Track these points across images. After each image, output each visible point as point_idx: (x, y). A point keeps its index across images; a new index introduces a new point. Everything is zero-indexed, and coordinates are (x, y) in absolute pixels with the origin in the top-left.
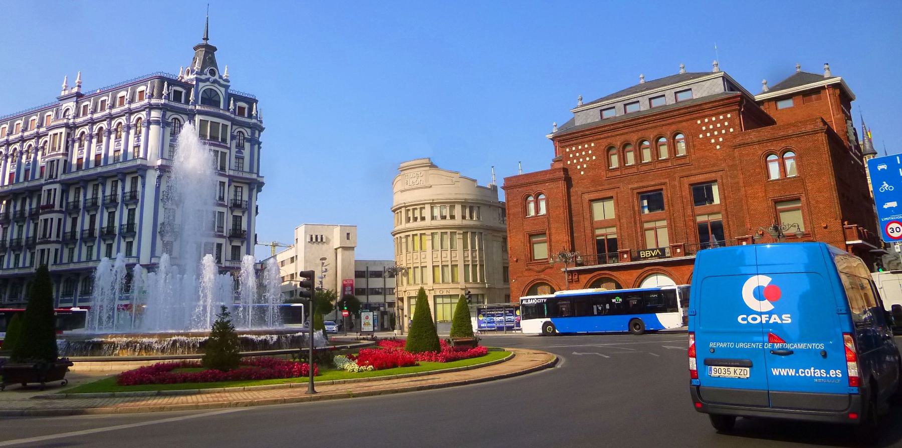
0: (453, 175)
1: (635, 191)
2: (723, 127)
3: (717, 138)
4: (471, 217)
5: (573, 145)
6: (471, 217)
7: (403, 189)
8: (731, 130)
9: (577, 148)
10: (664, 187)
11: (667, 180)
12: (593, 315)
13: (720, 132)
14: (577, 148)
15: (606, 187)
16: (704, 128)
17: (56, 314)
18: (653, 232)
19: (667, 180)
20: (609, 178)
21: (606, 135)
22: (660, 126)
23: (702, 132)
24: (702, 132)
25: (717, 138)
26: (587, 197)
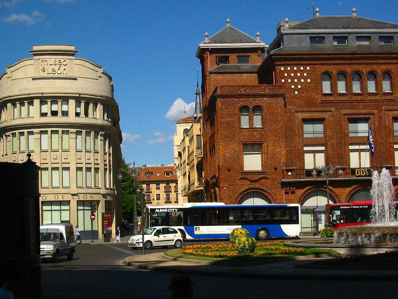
0: (97, 69)
1: (346, 117)
2: (289, 76)
3: (296, 85)
4: (86, 114)
5: (288, 65)
6: (86, 114)
7: (37, 75)
8: (309, 80)
9: (305, 68)
10: (372, 116)
11: (375, 111)
12: (78, 206)
13: (299, 81)
14: (305, 68)
15: (319, 109)
16: (286, 75)
17: (47, 248)
18: (357, 153)
19: (375, 111)
20: (323, 102)
21: (366, 61)
22: (341, 64)
23: (284, 77)
24: (284, 77)
25: (296, 85)
26: (301, 116)
